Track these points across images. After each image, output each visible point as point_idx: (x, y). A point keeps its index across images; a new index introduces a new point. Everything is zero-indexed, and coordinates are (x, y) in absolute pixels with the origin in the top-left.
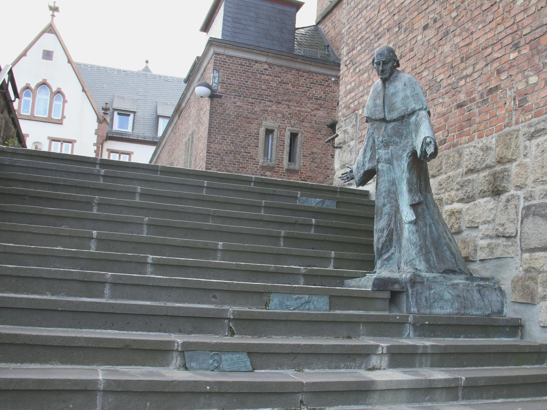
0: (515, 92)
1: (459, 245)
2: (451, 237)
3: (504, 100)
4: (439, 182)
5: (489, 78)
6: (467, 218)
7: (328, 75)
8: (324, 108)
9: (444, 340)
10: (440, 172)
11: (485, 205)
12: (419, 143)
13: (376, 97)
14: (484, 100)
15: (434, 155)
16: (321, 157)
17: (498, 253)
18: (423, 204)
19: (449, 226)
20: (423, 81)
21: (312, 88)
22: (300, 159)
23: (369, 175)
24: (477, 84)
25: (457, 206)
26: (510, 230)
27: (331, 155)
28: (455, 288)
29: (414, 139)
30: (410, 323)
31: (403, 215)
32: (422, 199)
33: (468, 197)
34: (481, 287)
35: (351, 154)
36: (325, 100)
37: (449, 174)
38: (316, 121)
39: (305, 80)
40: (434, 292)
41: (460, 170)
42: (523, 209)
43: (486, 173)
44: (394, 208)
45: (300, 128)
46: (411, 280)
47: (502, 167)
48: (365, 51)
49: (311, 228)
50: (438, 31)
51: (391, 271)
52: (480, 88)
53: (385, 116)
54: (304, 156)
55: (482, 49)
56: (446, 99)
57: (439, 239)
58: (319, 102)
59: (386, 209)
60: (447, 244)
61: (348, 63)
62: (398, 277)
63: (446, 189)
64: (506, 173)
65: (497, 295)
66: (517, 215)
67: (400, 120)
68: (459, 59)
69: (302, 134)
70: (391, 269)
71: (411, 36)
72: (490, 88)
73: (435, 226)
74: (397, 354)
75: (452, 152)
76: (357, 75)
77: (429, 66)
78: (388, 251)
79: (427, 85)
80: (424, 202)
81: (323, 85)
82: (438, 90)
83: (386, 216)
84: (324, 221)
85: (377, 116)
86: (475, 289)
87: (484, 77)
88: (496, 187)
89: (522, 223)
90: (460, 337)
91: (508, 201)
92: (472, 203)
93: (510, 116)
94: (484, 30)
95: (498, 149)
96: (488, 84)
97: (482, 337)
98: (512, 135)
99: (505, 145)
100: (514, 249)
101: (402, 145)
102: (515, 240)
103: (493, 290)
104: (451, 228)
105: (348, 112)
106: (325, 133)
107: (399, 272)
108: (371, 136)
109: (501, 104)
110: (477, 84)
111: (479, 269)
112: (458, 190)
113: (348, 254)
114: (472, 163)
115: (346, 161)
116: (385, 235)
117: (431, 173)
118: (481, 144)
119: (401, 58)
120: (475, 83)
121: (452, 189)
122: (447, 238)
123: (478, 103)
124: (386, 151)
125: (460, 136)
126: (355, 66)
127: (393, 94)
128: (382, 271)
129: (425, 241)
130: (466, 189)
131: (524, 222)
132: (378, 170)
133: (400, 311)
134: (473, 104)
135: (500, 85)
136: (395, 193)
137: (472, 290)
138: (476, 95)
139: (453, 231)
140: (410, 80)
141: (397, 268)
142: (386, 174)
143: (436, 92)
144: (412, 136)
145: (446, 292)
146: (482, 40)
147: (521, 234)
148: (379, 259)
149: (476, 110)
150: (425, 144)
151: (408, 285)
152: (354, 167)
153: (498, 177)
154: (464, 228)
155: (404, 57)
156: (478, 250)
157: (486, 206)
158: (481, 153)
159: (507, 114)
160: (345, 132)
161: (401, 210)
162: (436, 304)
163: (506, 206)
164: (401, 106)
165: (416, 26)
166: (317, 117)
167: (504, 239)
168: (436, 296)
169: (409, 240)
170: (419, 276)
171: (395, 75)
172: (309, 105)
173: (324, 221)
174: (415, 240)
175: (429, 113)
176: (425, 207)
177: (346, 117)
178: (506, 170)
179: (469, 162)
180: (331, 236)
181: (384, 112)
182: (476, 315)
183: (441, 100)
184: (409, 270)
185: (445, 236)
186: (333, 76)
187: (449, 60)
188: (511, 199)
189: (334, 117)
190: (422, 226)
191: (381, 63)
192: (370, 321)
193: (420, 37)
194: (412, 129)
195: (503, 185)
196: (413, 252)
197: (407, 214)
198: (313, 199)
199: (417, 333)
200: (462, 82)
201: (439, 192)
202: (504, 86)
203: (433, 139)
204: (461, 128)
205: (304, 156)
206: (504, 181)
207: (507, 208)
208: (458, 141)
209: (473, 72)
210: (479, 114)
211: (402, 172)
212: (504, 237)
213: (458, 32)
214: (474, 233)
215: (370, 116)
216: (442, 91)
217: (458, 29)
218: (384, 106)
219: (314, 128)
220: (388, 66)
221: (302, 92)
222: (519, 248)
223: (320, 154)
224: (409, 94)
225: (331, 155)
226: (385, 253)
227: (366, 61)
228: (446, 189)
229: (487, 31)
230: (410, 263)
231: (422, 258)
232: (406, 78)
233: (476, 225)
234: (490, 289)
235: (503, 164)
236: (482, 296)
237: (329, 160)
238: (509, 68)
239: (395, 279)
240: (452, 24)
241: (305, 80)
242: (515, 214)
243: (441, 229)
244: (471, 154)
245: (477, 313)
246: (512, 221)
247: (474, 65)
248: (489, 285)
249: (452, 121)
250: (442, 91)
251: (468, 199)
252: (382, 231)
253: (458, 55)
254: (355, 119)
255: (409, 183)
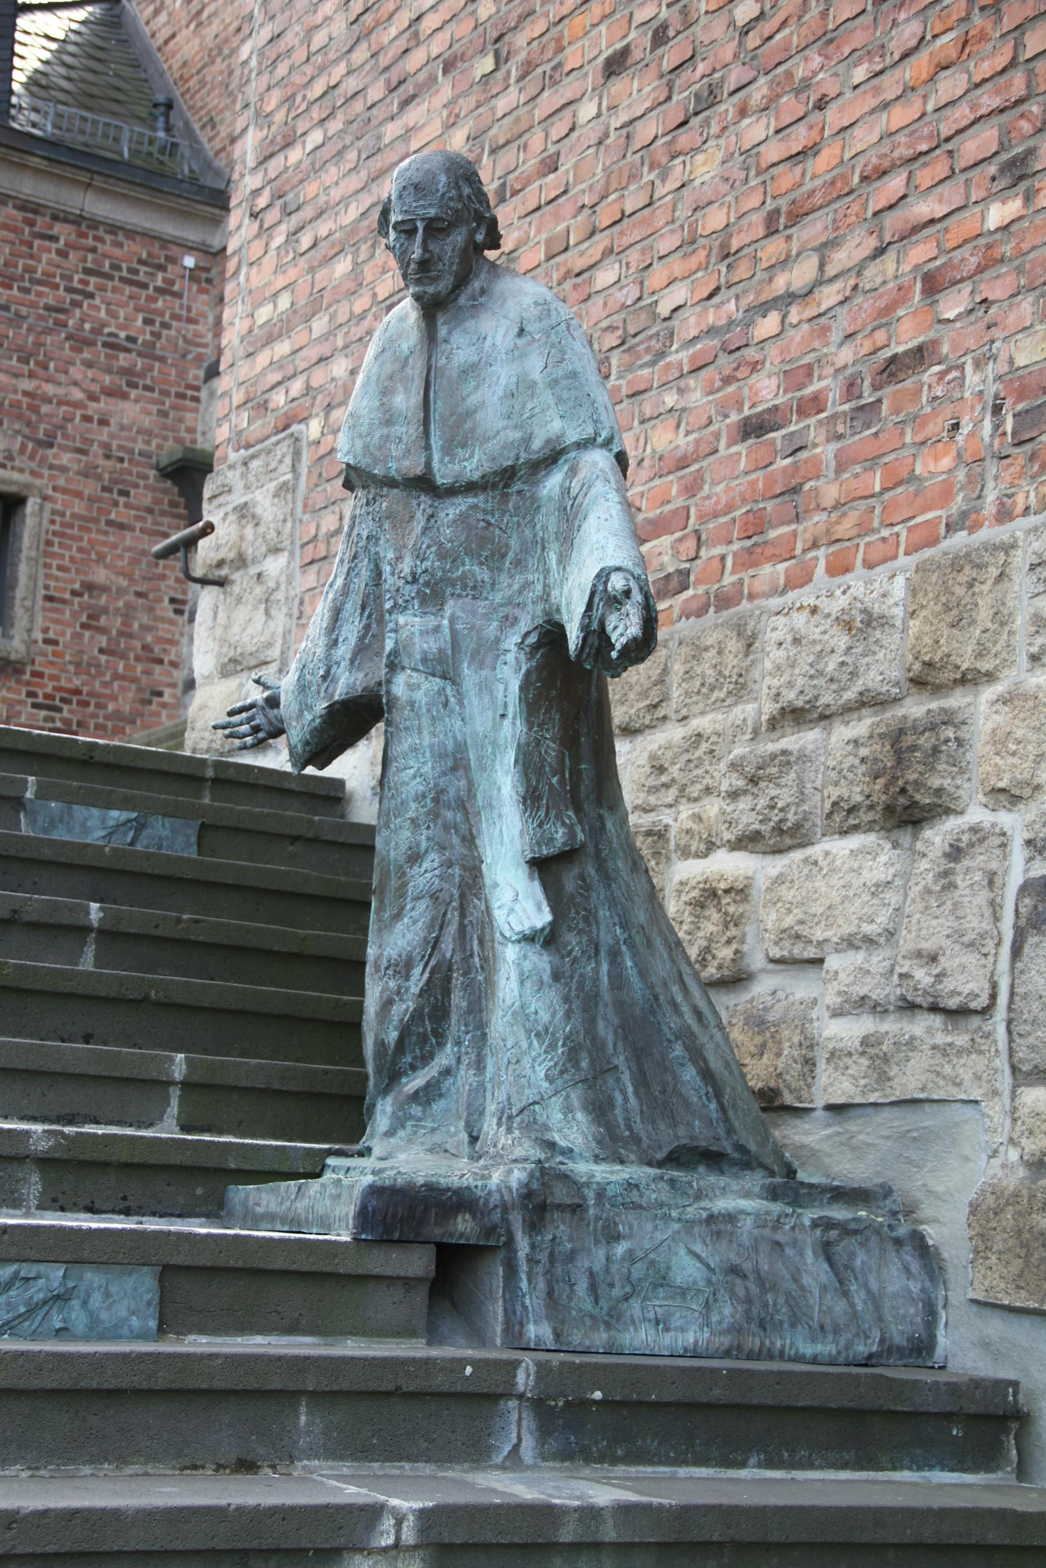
0: (999, 378)
1: (735, 1034)
2: (702, 1004)
3: (948, 410)
4: (653, 757)
5: (890, 309)
6: (771, 919)
7: (165, 242)
8: (146, 388)
9: (673, 1478)
10: (660, 712)
11: (853, 866)
12: (576, 593)
13: (391, 378)
14: (861, 408)
15: (642, 647)
16: (127, 605)
17: (909, 1080)
18: (587, 854)
19: (693, 953)
20: (596, 308)
21: (91, 296)
22: (30, 610)
23: (353, 718)
24: (835, 337)
25: (729, 865)
26: (965, 981)
27: (173, 601)
28: (718, 1234)
29: (554, 575)
30: (521, 1397)
31: (495, 904)
32: (581, 836)
33: (779, 830)
34: (834, 1234)
35: (267, 612)
36: (148, 352)
37: (702, 723)
38: (106, 446)
39: (62, 254)
40: (630, 1253)
41: (746, 711)
42: (1024, 889)
43: (861, 726)
44: (457, 871)
45: (33, 473)
46: (528, 1194)
47: (934, 705)
48: (340, 153)
49: (84, 943)
50: (670, 86)
51: (438, 1149)
52: (846, 355)
53: (428, 464)
54: (49, 598)
55: (864, 179)
56: (696, 397)
57: (653, 1012)
58: (123, 360)
59: (424, 876)
60: (686, 1035)
61: (262, 202)
62: (469, 1181)
63: (683, 789)
64: (950, 733)
65: (907, 1269)
66: (996, 919)
67: (494, 486)
68: (757, 219)
69: (45, 498)
70: (437, 1138)
71: (549, 101)
72: (888, 353)
73: (635, 955)
74: (465, 1546)
75: (711, 628)
76: (303, 263)
77: (626, 241)
78: (426, 1059)
79: (611, 328)
80: (591, 849)
81: (144, 286)
82: (661, 354)
83: (422, 905)
84: (137, 915)
85: (393, 465)
86: (809, 1240)
87: (866, 305)
88: (903, 791)
89: (1016, 952)
90: (743, 1464)
91: (955, 853)
92: (797, 855)
93: (976, 483)
94: (877, 91)
95: (914, 625)
96: (880, 337)
97: (844, 1466)
98: (979, 566)
99: (947, 608)
100: (980, 1067)
101: (498, 598)
102: (987, 1028)
103: (890, 1246)
104: (703, 962)
105: (259, 428)
106: (147, 500)
107: (475, 1157)
108: (365, 550)
109: (938, 426)
110: (835, 337)
111: (826, 1147)
112: (734, 795)
113: (250, 1067)
114: (800, 681)
115: (244, 652)
116: (415, 990)
117: (619, 715)
118: (842, 602)
119: (502, 200)
120: (825, 330)
121: (708, 791)
122: (685, 1009)
123: (834, 417)
124: (432, 621)
125: (750, 559)
126: (295, 220)
127: (470, 370)
128: (399, 1152)
129: (590, 1022)
130: (774, 792)
131: (1027, 950)
132: (392, 701)
133: (478, 1336)
134: (812, 421)
135: (935, 343)
136: (465, 805)
137: (795, 1243)
138: (826, 384)
139: (711, 971)
140: (544, 309)
141: (464, 1137)
142: (425, 721)
143: (653, 363)
144: (542, 560)
145: (682, 1251)
146: (864, 137)
147: (1011, 1001)
148: (385, 1092)
149: (826, 452)
150: (603, 598)
151: (517, 1221)
152: (286, 685)
153: (914, 748)
154: (757, 961)
155: (515, 193)
156: (821, 1064)
157: (858, 871)
158: (842, 641)
159: (961, 475)
160: (244, 513)
161: (488, 881)
162: (635, 1307)
163: (945, 874)
164: (501, 424)
165: (572, 58)
166: (113, 428)
167: (937, 1020)
168: (638, 1271)
169: (521, 1015)
170: (565, 1177)
171: (477, 285)
172: (76, 372)
173: (137, 915)
174: (545, 1017)
175: (621, 459)
176: (591, 870)
177: (248, 446)
178: (948, 718)
179: (786, 677)
180: (171, 981)
181: (428, 447)
182: (815, 1361)
183: (670, 399)
184: (519, 1152)
185: (679, 998)
186: (190, 249)
187: (715, 219)
188: (971, 845)
189: (191, 430)
190: (577, 952)
191: (420, 225)
192: (346, 1386)
193: (587, 110)
194: (545, 528)
195: (935, 782)
196: (538, 1069)
197: (516, 902)
198: (95, 812)
199: (552, 1445)
200: (768, 325)
201: (652, 800)
202: (954, 348)
203: (637, 579)
204: (755, 527)
205: (49, 598)
206: (942, 767)
207: (952, 886)
208: (741, 582)
209: (820, 282)
210: (840, 469)
211: (495, 715)
212: (934, 1009)
213: (758, 93)
214: (801, 988)
215: (364, 462)
216: (680, 357)
217: (762, 80)
218: (426, 422)
219: (99, 478)
220: (449, 244)
221: (48, 308)
222: (1002, 1063)
223: (121, 592)
224: (536, 375)
225: (173, 601)
226: (413, 1068)
227: (345, 201)
228: (683, 789)
229: (890, 95)
230: (523, 1117)
231: (575, 1096)
232: (528, 301)
233: (811, 953)
234: (874, 1240)
235: (938, 689)
236: (841, 1274)
237: (162, 620)
238: (980, 269)
239: (458, 1192)
240: (736, 56)
241: (62, 254)
242: (988, 913)
243: (661, 968)
244: (796, 641)
245: (819, 1348)
246: (971, 944)
247: (825, 249)
248: (869, 1220)
249: (714, 492)
250: (680, 357)
251: (781, 836)
252: (403, 968)
253: (754, 201)
254: (288, 461)
255: (529, 763)
